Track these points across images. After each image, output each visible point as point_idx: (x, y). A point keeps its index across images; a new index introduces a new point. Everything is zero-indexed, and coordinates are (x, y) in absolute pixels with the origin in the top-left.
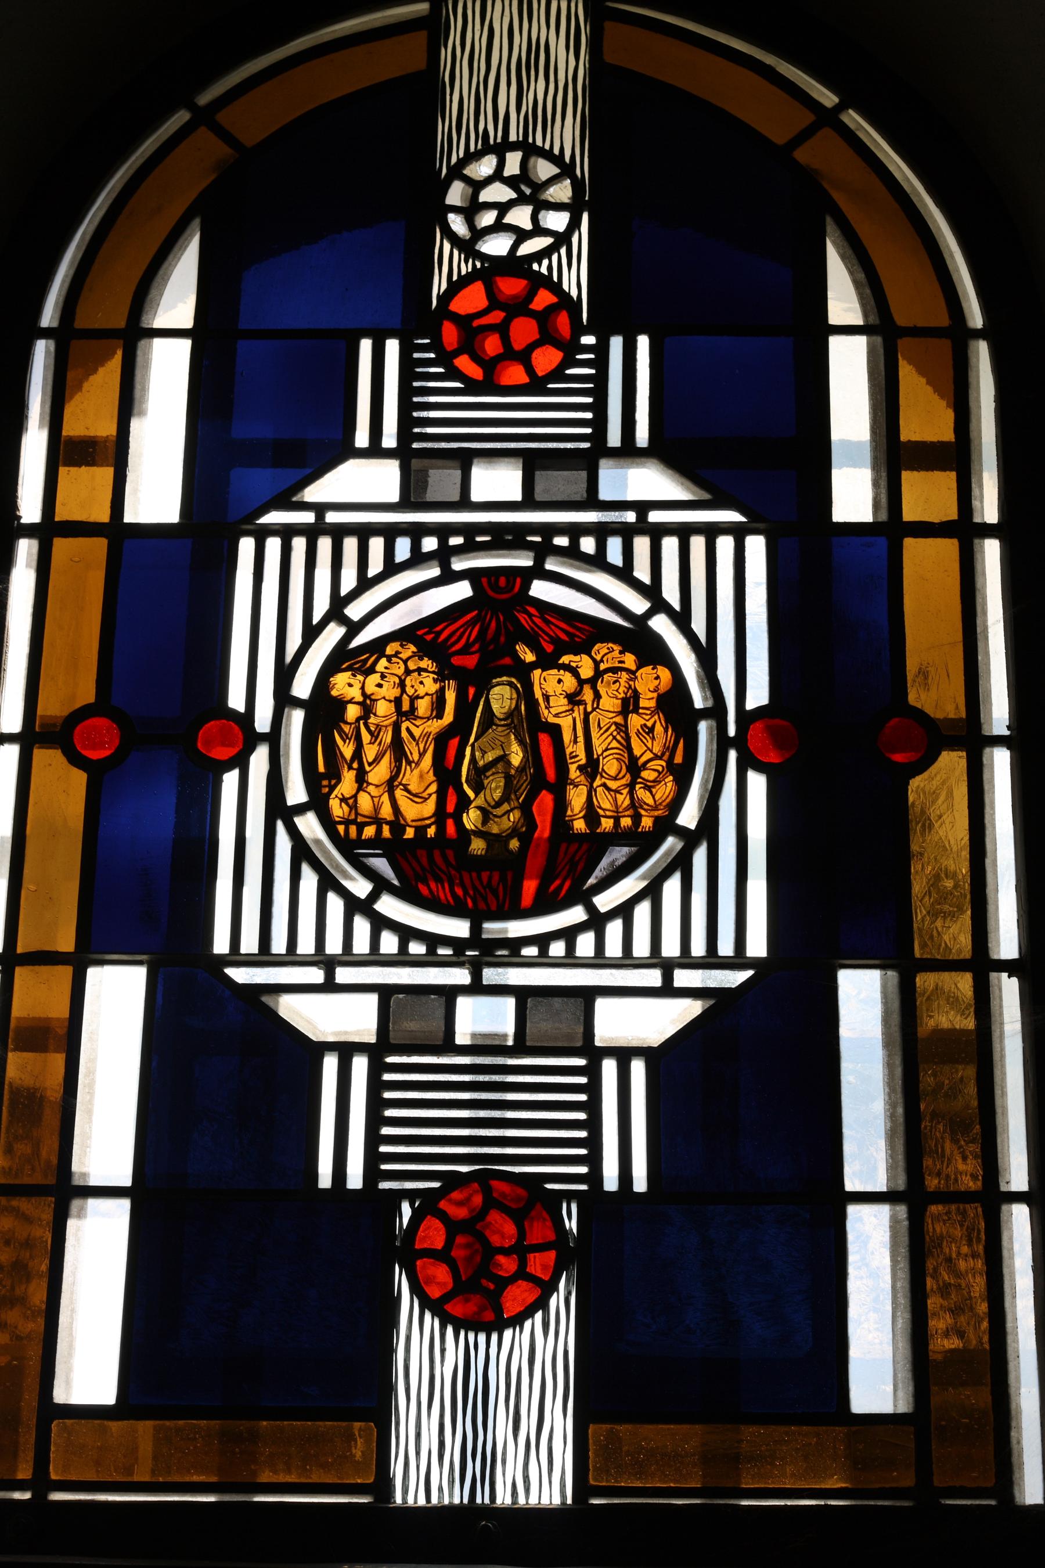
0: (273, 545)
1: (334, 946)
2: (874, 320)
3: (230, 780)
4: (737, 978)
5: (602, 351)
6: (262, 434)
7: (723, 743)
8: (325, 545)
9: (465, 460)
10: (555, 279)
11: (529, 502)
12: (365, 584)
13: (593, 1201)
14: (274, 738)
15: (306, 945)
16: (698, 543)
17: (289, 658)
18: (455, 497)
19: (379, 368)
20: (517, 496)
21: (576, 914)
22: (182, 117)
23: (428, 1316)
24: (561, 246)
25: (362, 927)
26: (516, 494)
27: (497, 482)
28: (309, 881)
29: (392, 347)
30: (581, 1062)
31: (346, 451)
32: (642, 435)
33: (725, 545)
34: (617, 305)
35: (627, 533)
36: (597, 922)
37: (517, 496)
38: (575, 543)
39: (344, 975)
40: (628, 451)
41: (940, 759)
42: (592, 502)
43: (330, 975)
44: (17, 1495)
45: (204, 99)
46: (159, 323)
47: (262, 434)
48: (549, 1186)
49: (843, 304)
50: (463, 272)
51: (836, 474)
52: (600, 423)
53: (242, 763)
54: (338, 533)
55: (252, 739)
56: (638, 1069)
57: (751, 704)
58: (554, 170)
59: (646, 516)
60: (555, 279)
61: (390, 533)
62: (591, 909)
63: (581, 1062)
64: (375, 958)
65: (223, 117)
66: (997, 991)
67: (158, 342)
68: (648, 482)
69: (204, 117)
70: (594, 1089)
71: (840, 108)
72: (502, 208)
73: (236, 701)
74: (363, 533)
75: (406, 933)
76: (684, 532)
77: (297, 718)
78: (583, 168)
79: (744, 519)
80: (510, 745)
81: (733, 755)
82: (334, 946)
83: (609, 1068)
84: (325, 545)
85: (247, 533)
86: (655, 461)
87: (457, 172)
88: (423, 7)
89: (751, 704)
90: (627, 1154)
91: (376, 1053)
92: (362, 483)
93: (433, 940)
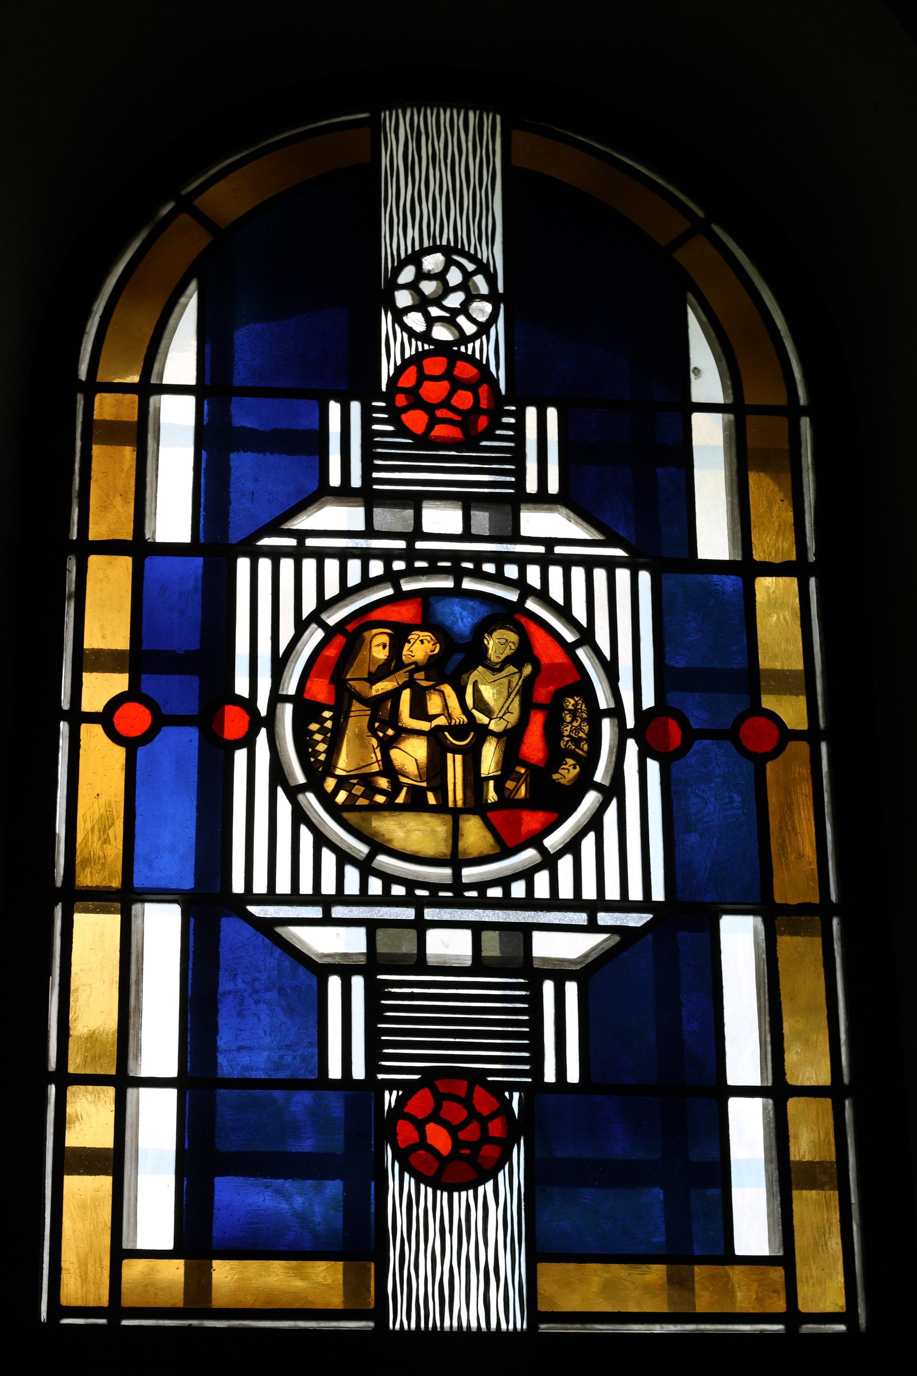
5: (521, 417)
6: (257, 460)
7: (623, 735)
8: (309, 565)
10: (484, 362)
11: (467, 535)
13: (535, 1089)
14: (270, 722)
15: (306, 888)
19: (342, 423)
21: (529, 855)
26: (458, 529)
32: (553, 487)
34: (531, 382)
36: (549, 862)
39: (338, 912)
40: (542, 499)
41: (788, 748)
44: (185, 1183)
47: (257, 460)
49: (707, 385)
51: (138, 1248)
53: (249, 743)
54: (320, 555)
56: (571, 988)
60: (484, 362)
62: (542, 850)
64: (364, 899)
68: (322, 942)
73: (242, 688)
74: (343, 555)
75: (499, 578)
76: (589, 563)
77: (287, 710)
78: (387, 322)
82: (328, 887)
84: (309, 565)
86: (564, 511)
90: (565, 1057)
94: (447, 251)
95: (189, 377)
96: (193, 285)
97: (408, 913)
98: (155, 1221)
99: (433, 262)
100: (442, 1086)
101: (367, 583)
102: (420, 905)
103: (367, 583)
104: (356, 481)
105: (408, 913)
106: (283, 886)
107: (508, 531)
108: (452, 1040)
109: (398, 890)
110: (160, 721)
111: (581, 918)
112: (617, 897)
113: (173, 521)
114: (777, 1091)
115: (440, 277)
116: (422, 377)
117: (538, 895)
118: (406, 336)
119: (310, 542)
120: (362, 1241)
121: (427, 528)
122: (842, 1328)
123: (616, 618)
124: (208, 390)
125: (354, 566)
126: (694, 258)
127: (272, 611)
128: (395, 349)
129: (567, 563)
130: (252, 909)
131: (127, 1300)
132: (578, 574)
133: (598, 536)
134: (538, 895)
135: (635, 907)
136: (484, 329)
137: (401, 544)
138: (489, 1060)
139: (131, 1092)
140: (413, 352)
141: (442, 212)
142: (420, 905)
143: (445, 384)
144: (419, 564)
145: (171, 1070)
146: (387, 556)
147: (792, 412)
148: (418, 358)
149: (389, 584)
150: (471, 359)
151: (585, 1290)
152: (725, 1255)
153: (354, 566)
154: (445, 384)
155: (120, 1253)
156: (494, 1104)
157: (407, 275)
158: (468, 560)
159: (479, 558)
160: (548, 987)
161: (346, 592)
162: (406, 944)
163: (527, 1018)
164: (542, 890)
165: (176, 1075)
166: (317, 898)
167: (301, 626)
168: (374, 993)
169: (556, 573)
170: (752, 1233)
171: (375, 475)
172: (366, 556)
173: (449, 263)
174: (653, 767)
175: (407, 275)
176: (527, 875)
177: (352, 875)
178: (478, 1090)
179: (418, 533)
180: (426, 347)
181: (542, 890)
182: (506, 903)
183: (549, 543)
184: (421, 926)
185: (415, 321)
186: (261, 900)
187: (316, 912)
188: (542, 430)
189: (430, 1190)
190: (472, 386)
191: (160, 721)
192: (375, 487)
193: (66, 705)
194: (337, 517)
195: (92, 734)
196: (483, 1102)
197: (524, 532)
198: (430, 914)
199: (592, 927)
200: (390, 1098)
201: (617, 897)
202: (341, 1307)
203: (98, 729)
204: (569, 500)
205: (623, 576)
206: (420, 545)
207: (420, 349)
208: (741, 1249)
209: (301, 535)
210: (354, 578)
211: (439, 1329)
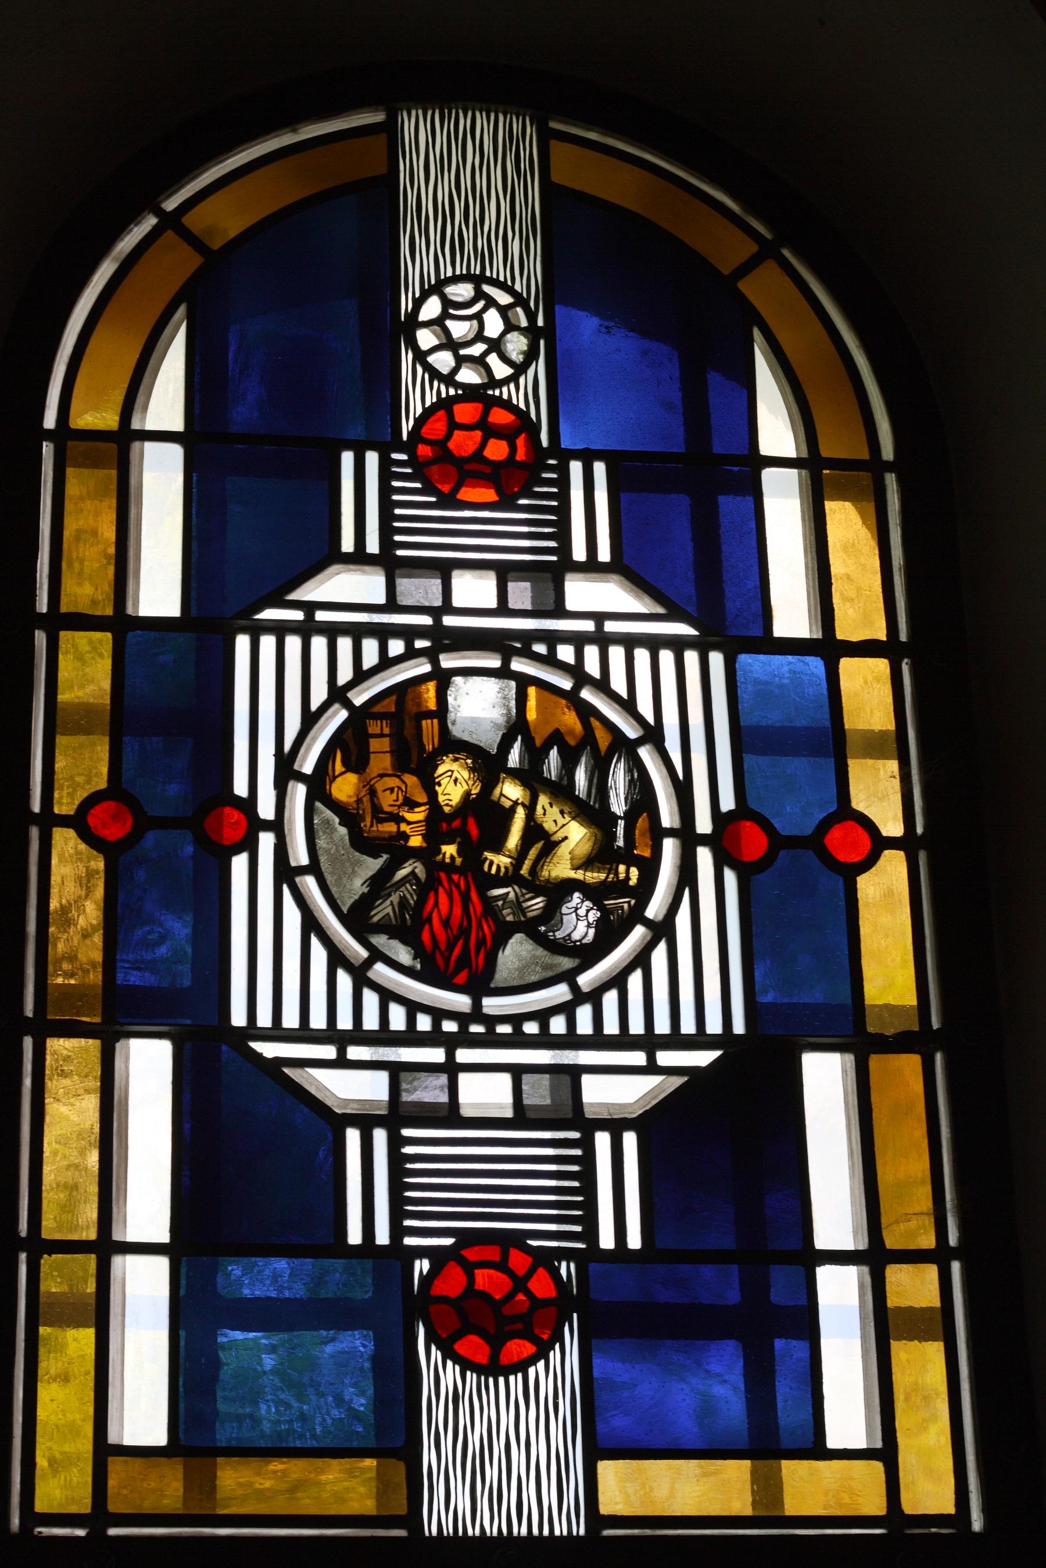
1: (345, 1022)
3: (239, 863)
4: (703, 1058)
8: (636, 1027)
9: (444, 570)
11: (503, 609)
13: (590, 1255)
14: (277, 826)
15: (318, 1021)
16: (291, 1020)
18: (527, 1079)
19: (358, 481)
20: (492, 603)
22: (151, 221)
23: (449, 1363)
24: (521, 375)
25: (592, 667)
27: (474, 590)
29: (372, 459)
30: (575, 1135)
31: (330, 556)
32: (604, 555)
33: (264, 1019)
37: (492, 603)
39: (355, 1053)
40: (592, 567)
42: (396, 1071)
43: (342, 1052)
46: (151, 425)
49: (776, 432)
52: (563, 534)
54: (332, 631)
61: (598, 1041)
63: (575, 1135)
64: (384, 1037)
67: (150, 447)
70: (588, 1161)
73: (241, 788)
74: (357, 633)
75: (551, 660)
78: (407, 359)
79: (697, 633)
83: (602, 1140)
85: (243, 630)
88: (379, 117)
90: (620, 1217)
91: (566, 565)
92: (616, 1090)
93: (438, 1014)
95: (176, 423)
96: (182, 311)
97: (436, 1055)
98: (143, 1415)
100: (472, 1254)
102: (451, 1043)
105: (436, 1055)
106: (291, 1020)
107: (550, 605)
109: (424, 1023)
111: (638, 1058)
114: (875, 1257)
120: (394, 1433)
121: (457, 602)
122: (402, 1533)
124: (196, 439)
126: (763, 289)
130: (258, 1046)
131: (114, 1506)
133: (661, 610)
136: (520, 369)
137: (426, 620)
139: (117, 1261)
140: (435, 400)
143: (478, 434)
146: (409, 633)
147: (875, 466)
148: (443, 405)
149: (499, 656)
150: (507, 405)
151: (632, 1488)
152: (816, 1448)
154: (478, 434)
155: (104, 1451)
157: (432, 308)
158: (517, 640)
159: (529, 637)
161: (361, 676)
164: (584, 1025)
166: (331, 1035)
167: (664, 930)
168: (395, 1143)
170: (847, 1421)
172: (382, 633)
174: (730, 878)
175: (432, 308)
176: (568, 1009)
179: (447, 607)
180: (452, 392)
181: (584, 1025)
182: (545, 1040)
184: (452, 1069)
185: (443, 361)
186: (266, 1036)
187: (329, 1052)
189: (475, 1376)
190: (506, 434)
193: (36, 808)
195: (65, 840)
197: (571, 605)
200: (422, 1266)
202: (374, 1512)
203: (71, 833)
204: (623, 567)
206: (449, 621)
207: (444, 395)
208: (833, 1442)
209: (310, 608)
210: (610, 999)
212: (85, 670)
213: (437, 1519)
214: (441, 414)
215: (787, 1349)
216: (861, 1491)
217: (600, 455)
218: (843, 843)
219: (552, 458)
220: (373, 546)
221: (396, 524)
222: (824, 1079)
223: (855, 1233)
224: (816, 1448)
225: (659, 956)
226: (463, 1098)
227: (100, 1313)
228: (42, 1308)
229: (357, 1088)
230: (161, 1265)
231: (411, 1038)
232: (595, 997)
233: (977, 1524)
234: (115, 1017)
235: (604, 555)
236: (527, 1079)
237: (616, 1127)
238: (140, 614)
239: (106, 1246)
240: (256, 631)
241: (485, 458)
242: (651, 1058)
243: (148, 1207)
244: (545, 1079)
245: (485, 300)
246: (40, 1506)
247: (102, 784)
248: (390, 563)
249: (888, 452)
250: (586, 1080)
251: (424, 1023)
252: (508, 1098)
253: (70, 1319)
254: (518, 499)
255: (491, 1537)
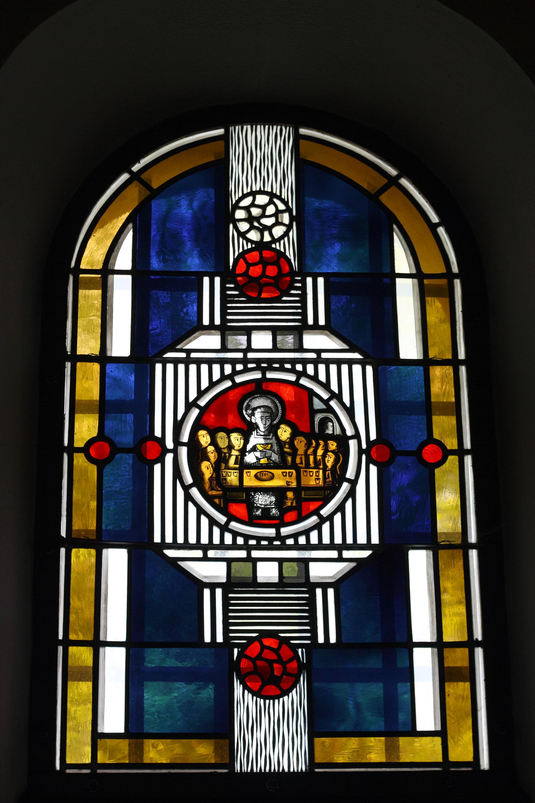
0: (170, 367)
1: (205, 540)
2: (414, 271)
3: (157, 468)
7: (361, 452)
9: (248, 331)
11: (275, 349)
12: (201, 393)
13: (313, 647)
14: (175, 451)
15: (192, 540)
17: (179, 417)
18: (285, 565)
19: (211, 290)
22: (125, 177)
27: (262, 340)
28: (192, 510)
29: (217, 280)
32: (322, 321)
35: (211, 546)
37: (270, 346)
38: (294, 367)
39: (211, 554)
40: (316, 327)
45: (136, 168)
48: (292, 642)
49: (402, 262)
50: (246, 248)
52: (304, 314)
54: (199, 362)
55: (166, 451)
56: (331, 592)
57: (372, 439)
58: (249, 236)
59: (457, 278)
64: (222, 546)
65: (144, 176)
66: (343, 571)
69: (135, 177)
71: (398, 177)
72: (263, 215)
73: (158, 433)
74: (210, 362)
76: (339, 362)
78: (293, 205)
79: (362, 357)
80: (211, 479)
81: (364, 457)
82: (205, 540)
85: (159, 362)
87: (236, 206)
89: (372, 439)
90: (328, 629)
92: (323, 571)
94: (272, 195)
95: (128, 266)
97: (242, 554)
98: (113, 720)
99: (262, 200)
101: (223, 378)
103: (223, 378)
104: (217, 321)
105: (242, 554)
108: (299, 621)
110: (418, 454)
111: (334, 554)
112: (341, 542)
113: (121, 345)
115: (264, 208)
116: (249, 265)
117: (359, 542)
118: (245, 242)
119: (193, 355)
120: (220, 726)
121: (254, 346)
123: (355, 392)
125: (216, 368)
127: (175, 392)
128: (235, 249)
129: (327, 362)
132: (333, 368)
134: (359, 542)
135: (362, 547)
137: (240, 355)
138: (290, 631)
141: (262, 165)
142: (248, 548)
144: (250, 366)
145: (123, 638)
146: (233, 362)
147: (449, 276)
151: (344, 751)
152: (413, 732)
153: (216, 368)
155: (97, 737)
156: (291, 654)
158: (276, 363)
160: (319, 592)
161: (212, 384)
162: (245, 570)
163: (307, 608)
165: (444, 641)
166: (198, 546)
167: (189, 406)
169: (322, 368)
170: (426, 718)
171: (229, 317)
172: (222, 362)
173: (271, 202)
176: (318, 527)
177: (216, 531)
178: (284, 647)
179: (249, 349)
182: (296, 547)
183: (318, 352)
187: (199, 554)
188: (316, 290)
191: (418, 454)
192: (229, 324)
194: (210, 341)
196: (286, 653)
198: (255, 554)
199: (340, 559)
201: (341, 542)
205: (357, 369)
206: (250, 355)
210: (216, 376)
211: (263, 771)
212: (88, 383)
213: (241, 765)
214: (241, 260)
215: (402, 687)
216: (427, 751)
217: (321, 275)
218: (430, 454)
219: (298, 276)
220: (217, 321)
221: (229, 311)
222: (419, 561)
223: (432, 633)
224: (413, 732)
225: (193, 395)
226: (259, 574)
227: (94, 675)
228: (70, 673)
229: (213, 571)
230: (122, 651)
231: (234, 546)
232: (330, 518)
233: (485, 763)
234: (99, 542)
235: (322, 321)
236: (285, 565)
237: (325, 586)
238: (113, 356)
239: (97, 644)
240: (165, 362)
241: (264, 280)
242: (340, 554)
243: (116, 626)
244: (294, 564)
245: (319, 587)
246: (69, 761)
247: (437, 471)
248: (224, 330)
249: (455, 269)
250: (312, 565)
251: (240, 541)
252: (276, 574)
253: (81, 678)
254: (282, 297)
255: (257, 772)
